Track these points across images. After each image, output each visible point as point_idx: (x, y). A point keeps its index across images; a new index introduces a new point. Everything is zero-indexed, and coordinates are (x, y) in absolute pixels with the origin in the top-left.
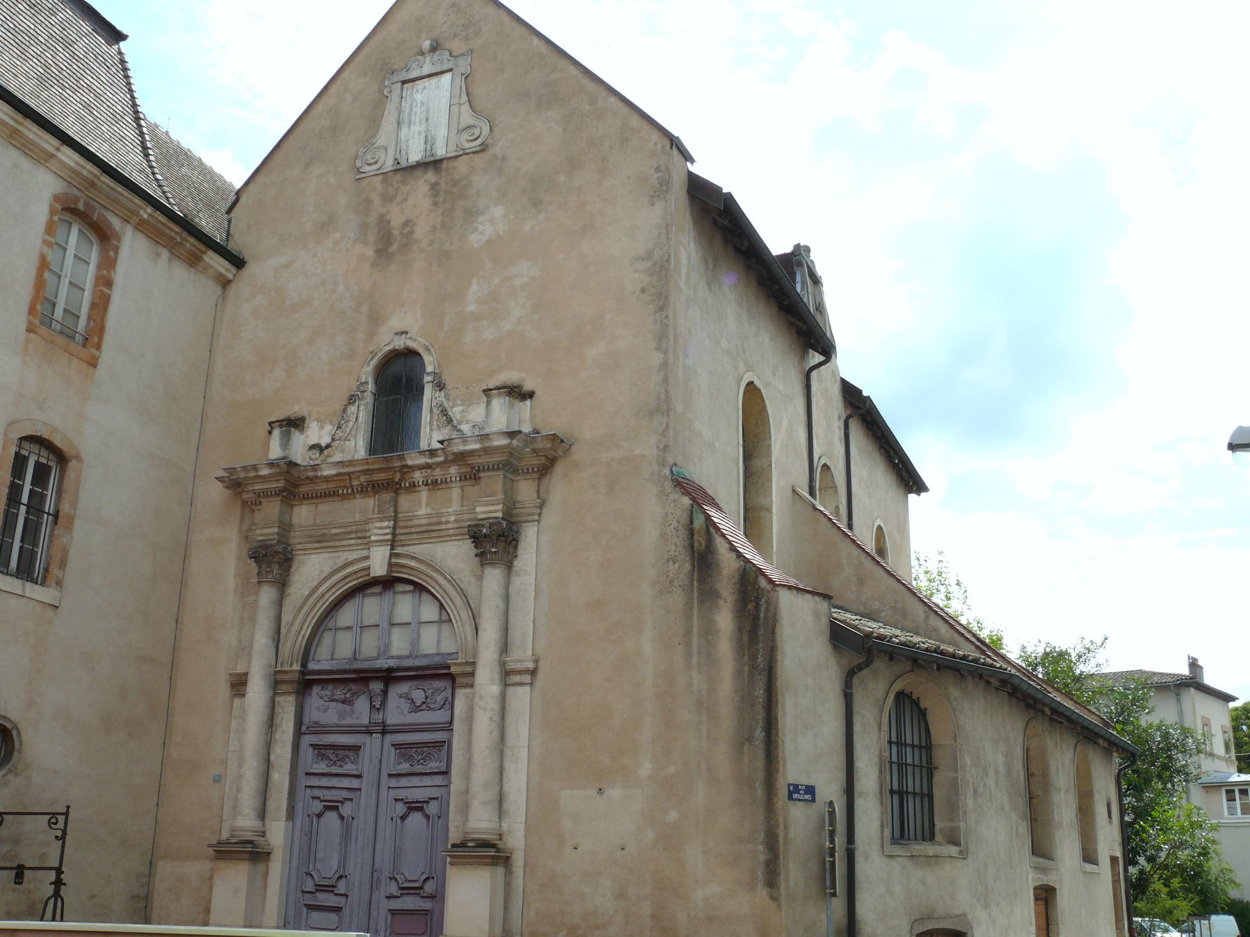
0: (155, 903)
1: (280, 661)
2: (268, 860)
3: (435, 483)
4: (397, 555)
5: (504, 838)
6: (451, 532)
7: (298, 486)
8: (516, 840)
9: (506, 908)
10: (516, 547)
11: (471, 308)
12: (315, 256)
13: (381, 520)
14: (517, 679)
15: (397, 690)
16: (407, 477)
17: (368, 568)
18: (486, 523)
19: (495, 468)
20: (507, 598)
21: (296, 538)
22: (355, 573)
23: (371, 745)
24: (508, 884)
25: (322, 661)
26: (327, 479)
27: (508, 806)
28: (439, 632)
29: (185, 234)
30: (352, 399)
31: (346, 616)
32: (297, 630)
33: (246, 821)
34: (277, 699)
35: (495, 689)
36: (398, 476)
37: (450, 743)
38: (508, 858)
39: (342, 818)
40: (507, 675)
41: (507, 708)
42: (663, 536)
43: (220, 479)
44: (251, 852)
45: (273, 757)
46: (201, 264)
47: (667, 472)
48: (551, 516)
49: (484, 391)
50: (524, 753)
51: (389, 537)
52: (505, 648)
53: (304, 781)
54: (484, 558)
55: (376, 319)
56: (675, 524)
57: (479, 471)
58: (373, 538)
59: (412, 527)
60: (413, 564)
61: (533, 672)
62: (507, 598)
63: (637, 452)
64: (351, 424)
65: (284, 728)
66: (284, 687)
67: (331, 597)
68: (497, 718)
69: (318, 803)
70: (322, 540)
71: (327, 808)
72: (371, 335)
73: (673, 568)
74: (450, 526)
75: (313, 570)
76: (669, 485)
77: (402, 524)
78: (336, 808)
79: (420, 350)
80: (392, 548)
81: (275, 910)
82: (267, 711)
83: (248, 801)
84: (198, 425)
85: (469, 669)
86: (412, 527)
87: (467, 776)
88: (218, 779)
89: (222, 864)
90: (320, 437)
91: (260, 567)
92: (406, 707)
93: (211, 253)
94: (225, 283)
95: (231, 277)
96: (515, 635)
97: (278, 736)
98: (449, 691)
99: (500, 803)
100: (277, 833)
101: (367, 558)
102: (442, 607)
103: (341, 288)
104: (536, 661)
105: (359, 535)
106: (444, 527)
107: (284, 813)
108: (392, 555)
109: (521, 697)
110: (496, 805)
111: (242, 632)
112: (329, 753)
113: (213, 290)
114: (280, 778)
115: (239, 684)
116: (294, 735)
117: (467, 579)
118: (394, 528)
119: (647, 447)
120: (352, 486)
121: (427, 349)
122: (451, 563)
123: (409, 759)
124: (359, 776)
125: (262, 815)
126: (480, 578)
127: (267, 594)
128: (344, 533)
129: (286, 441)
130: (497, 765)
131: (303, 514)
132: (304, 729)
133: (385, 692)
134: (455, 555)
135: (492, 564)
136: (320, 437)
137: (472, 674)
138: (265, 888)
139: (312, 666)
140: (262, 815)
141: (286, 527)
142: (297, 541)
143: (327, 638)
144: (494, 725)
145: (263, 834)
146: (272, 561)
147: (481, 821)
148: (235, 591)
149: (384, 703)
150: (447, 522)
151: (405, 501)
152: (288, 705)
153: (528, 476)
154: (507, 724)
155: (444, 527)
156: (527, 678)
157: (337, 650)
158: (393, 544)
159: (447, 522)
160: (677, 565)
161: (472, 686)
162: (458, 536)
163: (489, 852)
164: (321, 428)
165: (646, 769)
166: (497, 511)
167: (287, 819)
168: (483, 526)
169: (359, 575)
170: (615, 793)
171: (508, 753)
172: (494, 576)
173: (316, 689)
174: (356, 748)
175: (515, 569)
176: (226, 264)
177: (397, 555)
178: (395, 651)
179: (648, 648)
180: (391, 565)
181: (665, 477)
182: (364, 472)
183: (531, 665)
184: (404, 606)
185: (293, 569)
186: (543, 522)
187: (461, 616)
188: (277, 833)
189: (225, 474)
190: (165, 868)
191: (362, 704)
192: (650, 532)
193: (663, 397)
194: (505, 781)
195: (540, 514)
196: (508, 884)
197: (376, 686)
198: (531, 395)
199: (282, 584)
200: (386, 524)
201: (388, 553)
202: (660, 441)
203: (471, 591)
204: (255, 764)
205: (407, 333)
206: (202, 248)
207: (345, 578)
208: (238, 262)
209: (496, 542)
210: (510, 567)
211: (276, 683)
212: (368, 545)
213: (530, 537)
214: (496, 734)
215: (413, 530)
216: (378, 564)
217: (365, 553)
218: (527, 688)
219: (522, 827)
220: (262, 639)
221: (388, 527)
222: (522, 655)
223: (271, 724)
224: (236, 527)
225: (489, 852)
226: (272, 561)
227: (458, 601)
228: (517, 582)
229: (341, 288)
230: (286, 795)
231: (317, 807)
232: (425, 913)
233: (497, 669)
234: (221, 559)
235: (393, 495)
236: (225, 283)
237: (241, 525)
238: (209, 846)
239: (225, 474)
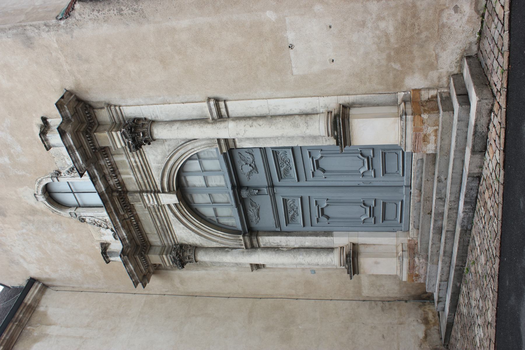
0: (386, 295)
1: (240, 247)
2: (357, 244)
3: (114, 171)
4: (163, 189)
5: (330, 110)
6: (141, 159)
7: (137, 246)
8: (332, 103)
9: (378, 105)
10: (139, 119)
11: (7, 160)
12: (12, 245)
13: (144, 200)
14: (223, 111)
15: (245, 180)
16: (114, 189)
17: (175, 205)
18: (126, 141)
19: (92, 140)
20: (172, 122)
21: (168, 242)
22: (179, 211)
23: (281, 193)
24: (361, 105)
25: (235, 222)
26: (129, 231)
27: (308, 109)
28: (205, 159)
29: (14, 320)
30: (83, 220)
31: (208, 212)
32: (220, 238)
33: (334, 260)
34: (262, 246)
35: (231, 124)
36: (115, 194)
37: (272, 148)
38: (343, 106)
39: (322, 157)
40: (221, 117)
41: (243, 115)
42: (106, 20)
43: (144, 286)
44: (352, 259)
45: (296, 246)
46: (33, 305)
47: (62, 22)
48: (114, 98)
49: (48, 150)
50: (272, 102)
51: (153, 194)
52: (202, 120)
53: (308, 228)
54: (150, 140)
55: (34, 211)
56: (95, 13)
57: (95, 149)
58: (156, 203)
59: (144, 182)
60: (166, 180)
61: (217, 101)
62: (172, 122)
63: (56, 45)
64: (96, 220)
65: (278, 241)
66: (255, 243)
67: (197, 222)
68: (250, 122)
69: (319, 220)
70: (166, 229)
71: (323, 214)
72: (44, 213)
73: (126, 11)
74: (137, 160)
75: (183, 233)
76: (70, 20)
77: (144, 188)
78: (317, 161)
79: (41, 186)
80: (159, 192)
81: (386, 239)
82: (270, 252)
83: (324, 259)
84: (121, 295)
85: (222, 142)
86: (144, 182)
87: (292, 138)
88: (314, 272)
89: (361, 271)
90: (109, 234)
91: (188, 262)
92: (254, 175)
93: (26, 300)
94: (45, 287)
95: (40, 285)
96: (195, 114)
97: (283, 244)
98: (240, 151)
99: (307, 114)
100: (341, 240)
101: (169, 205)
102: (190, 159)
103: (24, 231)
104: (209, 99)
105: (157, 210)
106: (139, 164)
107: (329, 238)
108: (164, 192)
109: (235, 107)
110: (308, 118)
111: (226, 265)
112: (290, 215)
113: (49, 294)
114: (308, 241)
115: (258, 267)
116: (282, 235)
117: (167, 147)
118: (147, 192)
119: (49, 38)
120: (130, 218)
121: (40, 183)
122: (159, 158)
123: (287, 171)
124: (302, 198)
125: (330, 250)
126: (164, 141)
127: (202, 257)
128: (158, 218)
129: (113, 253)
130: (281, 119)
131: (154, 239)
132: (279, 230)
133: (248, 188)
134: (155, 156)
135: (151, 134)
136: (109, 234)
137: (226, 140)
138: (374, 245)
139: (240, 228)
140: (330, 250)
141: (164, 250)
142: (170, 242)
143: (223, 221)
144: (255, 123)
145: (342, 248)
146: (183, 255)
147: (318, 131)
148: (207, 270)
149: (255, 188)
150: (136, 162)
151: (132, 186)
152: (265, 240)
153: (93, 116)
154: (254, 114)
155: (139, 164)
156: (222, 104)
157: (229, 215)
158: (156, 192)
159: (136, 162)
160: (124, 8)
161: (234, 139)
162: (143, 156)
163: (340, 123)
164: (104, 234)
165: (270, 15)
166: (117, 135)
167: (332, 236)
168: (128, 143)
169: (181, 208)
170: (291, 36)
171: (273, 112)
172: (158, 132)
173: (254, 225)
174: (285, 201)
175: (153, 118)
176: (32, 289)
177: (163, 189)
178: (223, 183)
179: (184, 23)
180: (170, 192)
181: (66, 23)
182: (118, 214)
183: (212, 103)
184: (194, 181)
185: (187, 243)
186: (120, 103)
187: (191, 149)
188: (341, 240)
189: (140, 285)
190: (366, 292)
191: (258, 200)
192: (106, 30)
193: (15, 31)
194: (292, 112)
195: (115, 106)
196: (361, 105)
197: (244, 194)
198: (44, 119)
199: (196, 248)
200: (145, 198)
201: (162, 194)
202: (43, 30)
203: (173, 144)
204: (301, 257)
205: (35, 194)
206: (23, 305)
207: (184, 216)
208: (32, 282)
209: (138, 133)
210: (153, 122)
211: (253, 247)
212: (162, 206)
213: (131, 111)
214: (261, 122)
215: (146, 181)
216: (170, 199)
217: (167, 207)
218: (228, 103)
219: (321, 99)
220: (228, 258)
221: (147, 196)
222: (204, 109)
223: (276, 249)
224: (172, 272)
225: (340, 123)
226: (183, 255)
227: (182, 151)
228: (161, 117)
229: (24, 231)
230: (318, 238)
231: (319, 172)
232: (384, 155)
233: (218, 125)
234: (189, 277)
235: (128, 193)
236: (45, 287)
237: (169, 270)
238: (351, 279)
239: (140, 285)
